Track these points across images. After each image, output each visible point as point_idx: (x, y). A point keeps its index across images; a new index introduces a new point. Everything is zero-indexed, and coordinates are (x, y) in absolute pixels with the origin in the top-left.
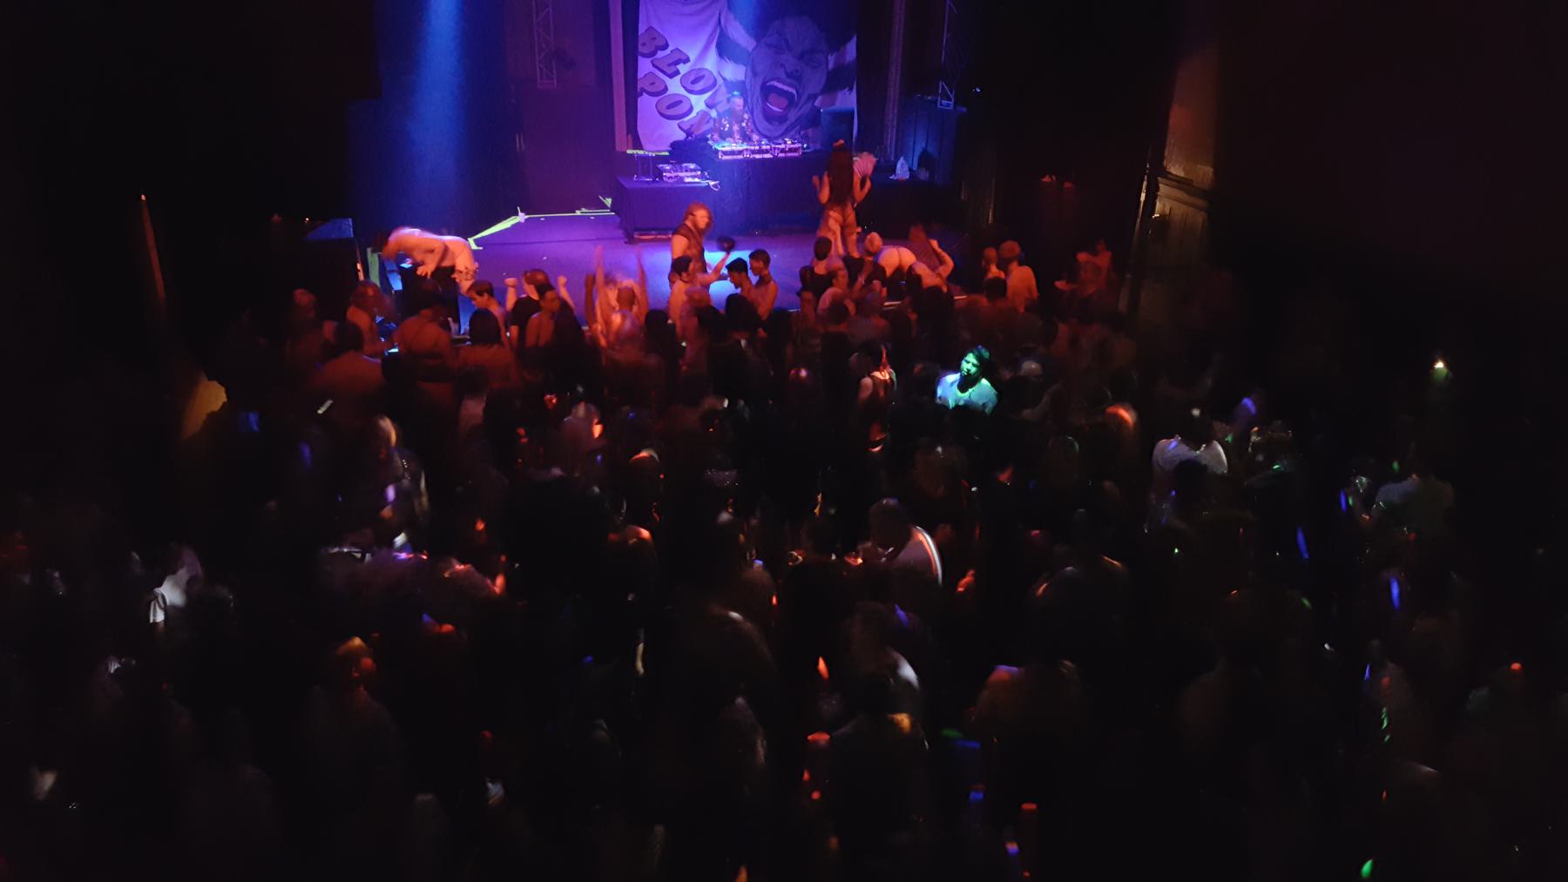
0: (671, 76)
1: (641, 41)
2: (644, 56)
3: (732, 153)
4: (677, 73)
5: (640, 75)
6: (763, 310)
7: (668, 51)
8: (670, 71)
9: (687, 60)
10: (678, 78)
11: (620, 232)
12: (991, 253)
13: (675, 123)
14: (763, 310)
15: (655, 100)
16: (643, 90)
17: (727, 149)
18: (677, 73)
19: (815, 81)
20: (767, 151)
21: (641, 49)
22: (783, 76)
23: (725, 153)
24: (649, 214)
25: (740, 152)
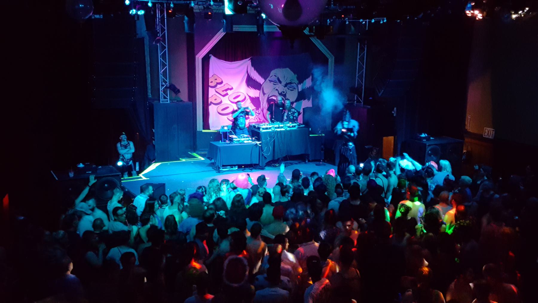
0: (224, 96)
1: (210, 81)
2: (212, 87)
3: (267, 129)
4: (227, 94)
5: (210, 96)
6: (256, 183)
7: (222, 85)
8: (223, 93)
9: (232, 89)
10: (227, 96)
11: (284, 155)
12: (443, 170)
13: (225, 117)
14: (256, 183)
15: (215, 107)
16: (211, 103)
17: (264, 127)
18: (227, 94)
19: (292, 96)
20: (282, 127)
21: (210, 84)
22: (277, 94)
23: (263, 129)
24: (214, 149)
25: (270, 128)
